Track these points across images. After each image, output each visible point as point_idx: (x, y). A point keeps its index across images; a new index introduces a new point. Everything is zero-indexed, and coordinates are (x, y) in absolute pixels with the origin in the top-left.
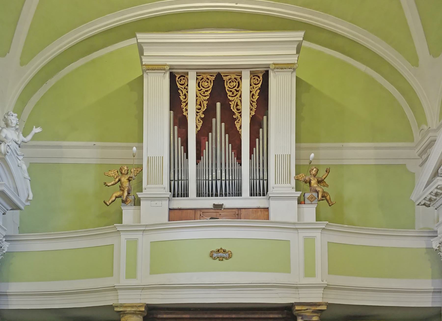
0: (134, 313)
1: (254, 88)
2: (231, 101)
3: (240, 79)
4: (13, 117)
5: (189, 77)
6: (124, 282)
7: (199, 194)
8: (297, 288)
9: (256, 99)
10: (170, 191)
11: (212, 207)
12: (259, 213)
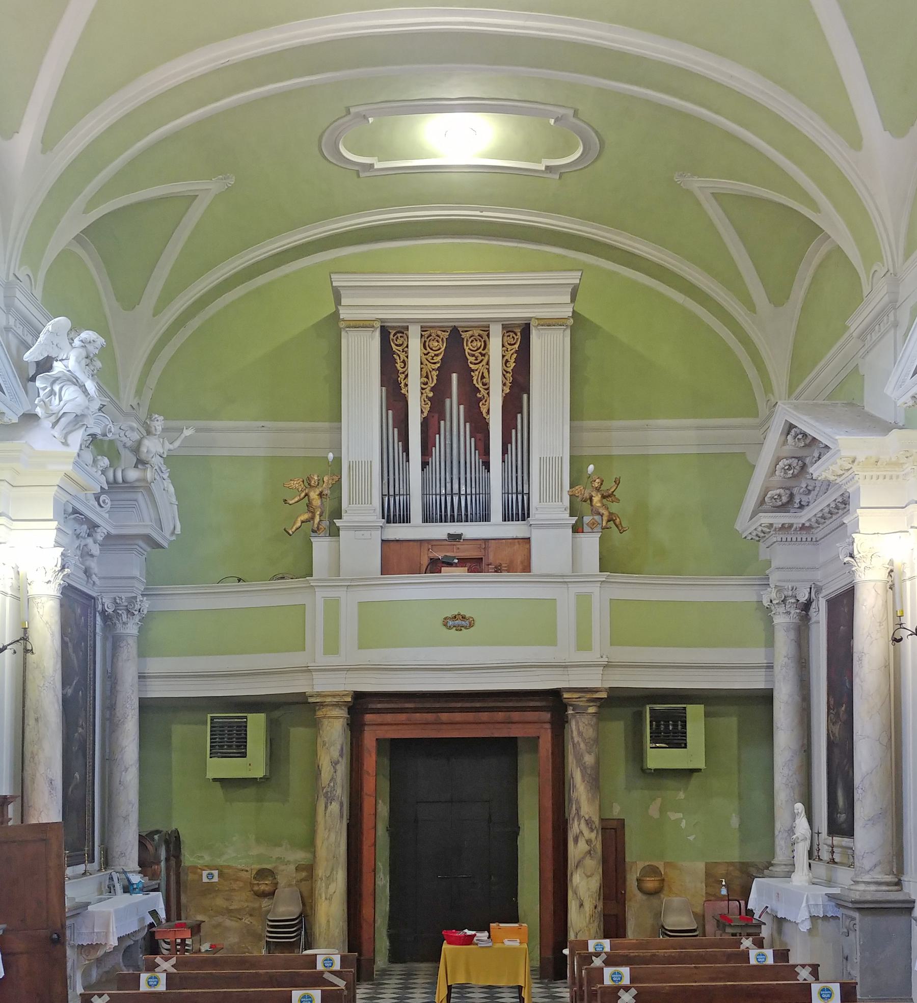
0: (337, 705)
1: (509, 350)
2: (473, 371)
3: (486, 337)
4: (159, 423)
5: (410, 333)
6: (323, 660)
7: (427, 518)
8: (566, 667)
9: (512, 368)
10: (383, 518)
11: (445, 537)
12: (516, 547)
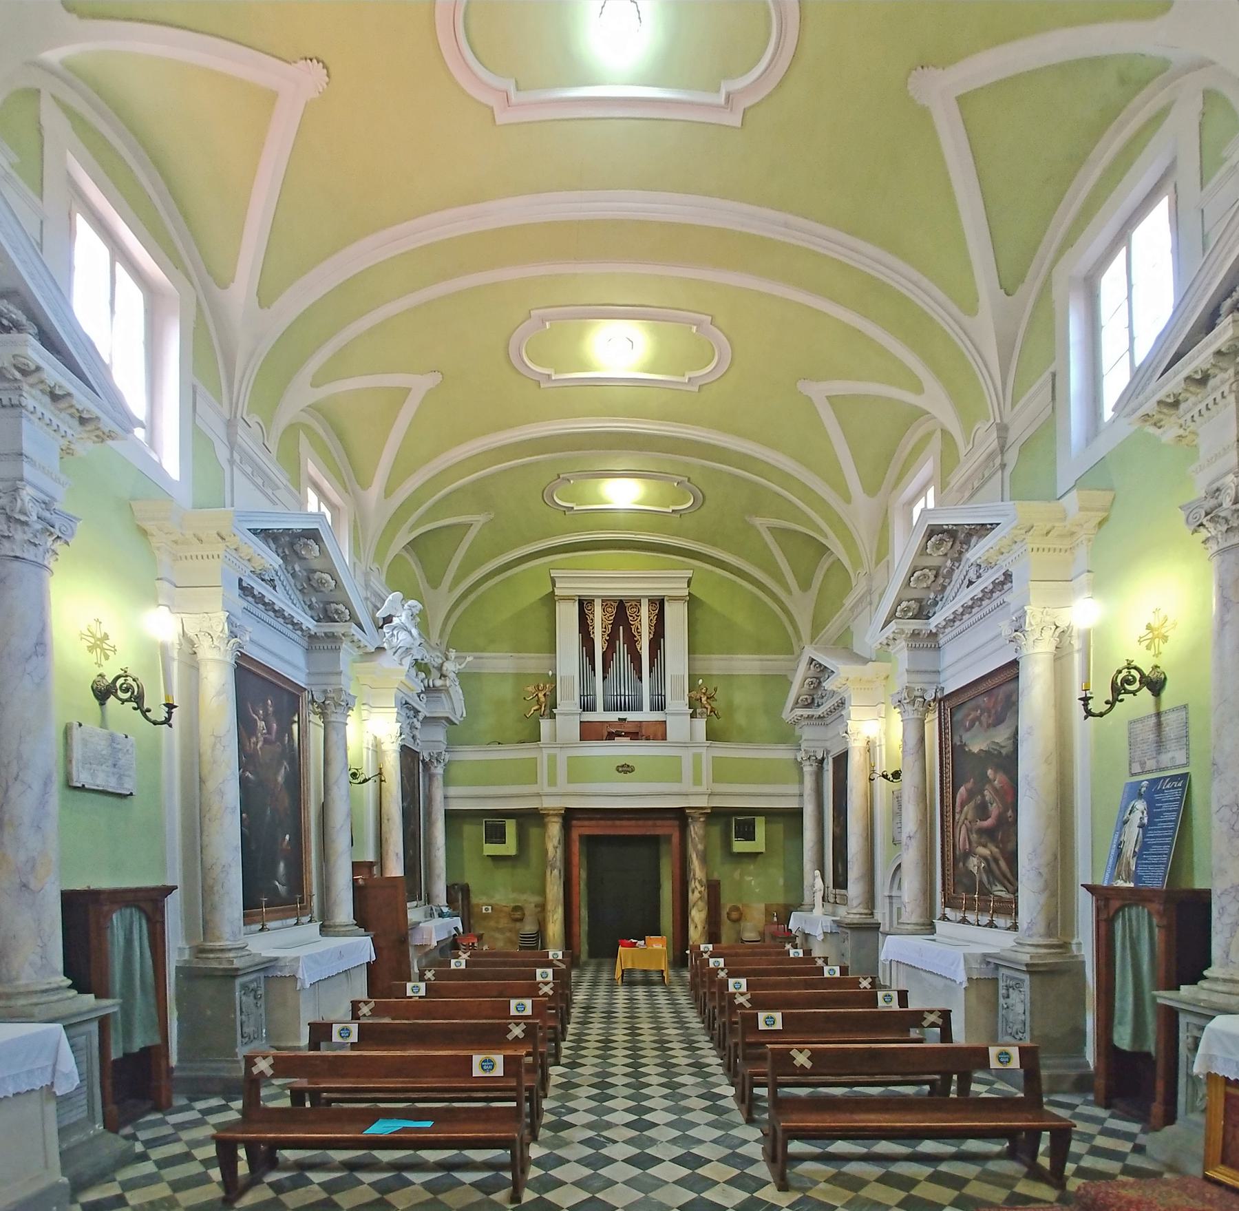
0: (556, 815)
6: (547, 790)
8: (687, 795)
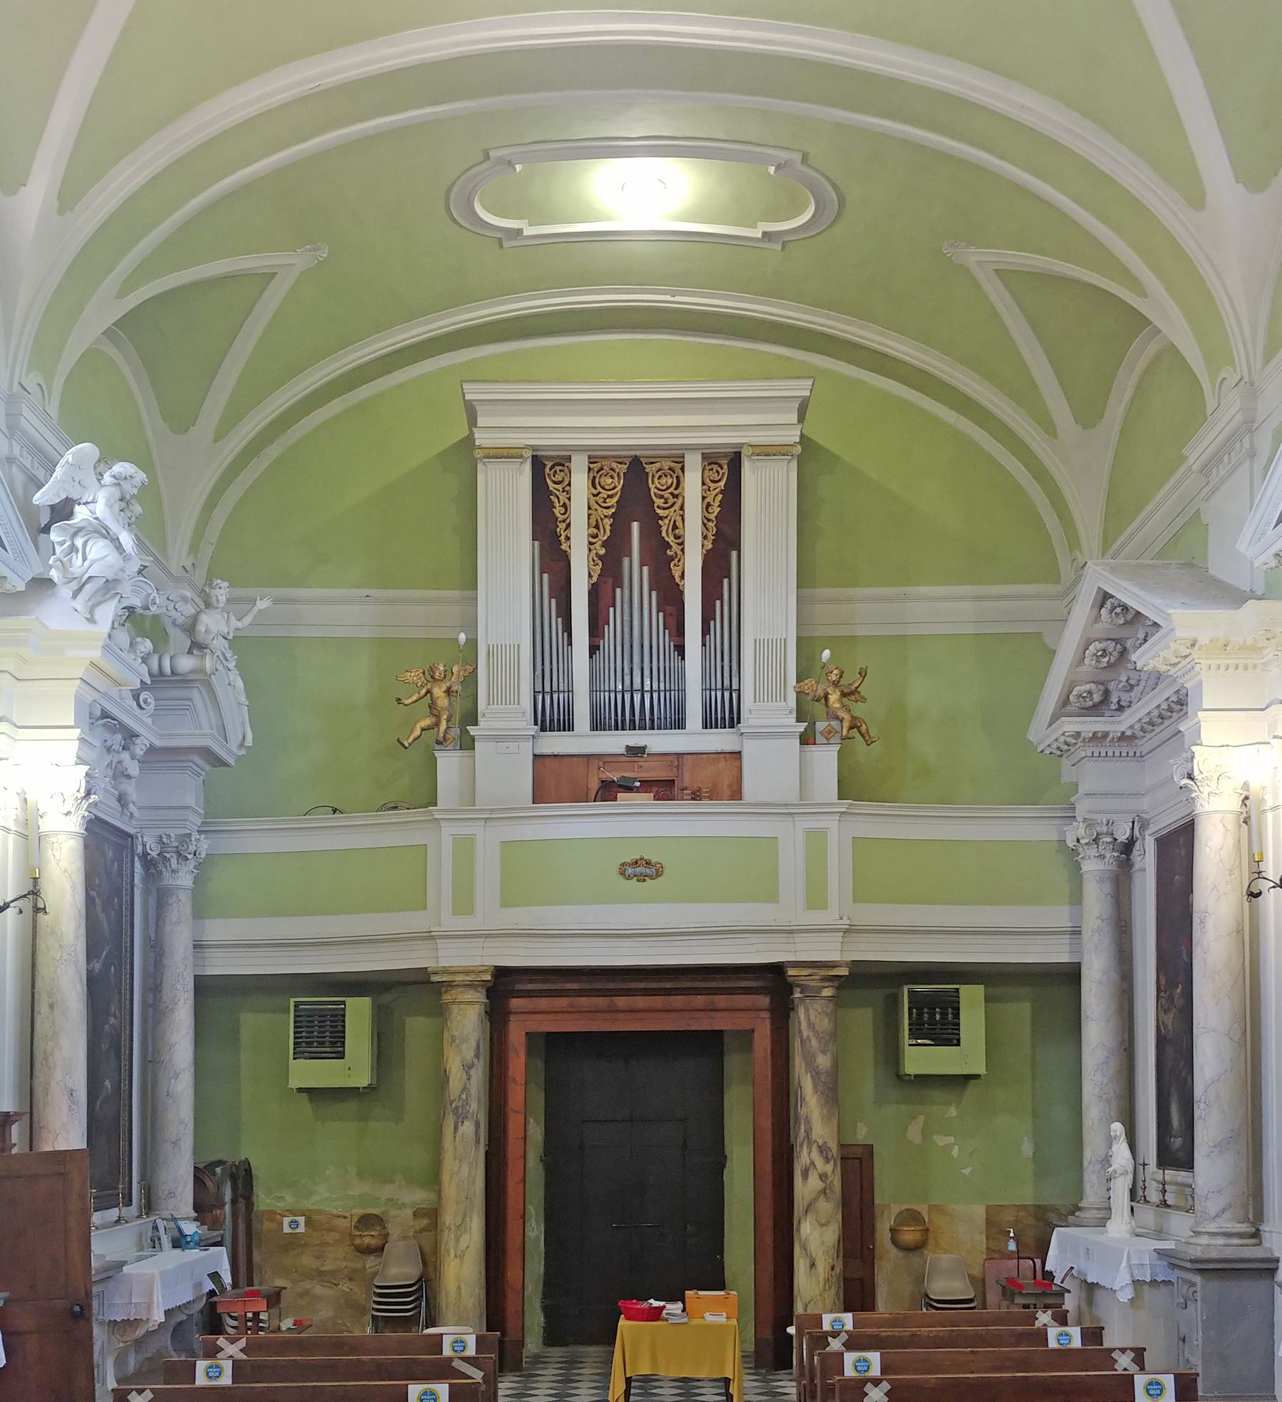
0: (471, 985)
1: (711, 489)
2: (661, 518)
3: (680, 471)
4: (222, 591)
5: (573, 465)
6: (451, 923)
7: (597, 725)
8: (791, 932)
9: (715, 514)
10: (536, 724)
11: (623, 751)
12: (722, 764)
